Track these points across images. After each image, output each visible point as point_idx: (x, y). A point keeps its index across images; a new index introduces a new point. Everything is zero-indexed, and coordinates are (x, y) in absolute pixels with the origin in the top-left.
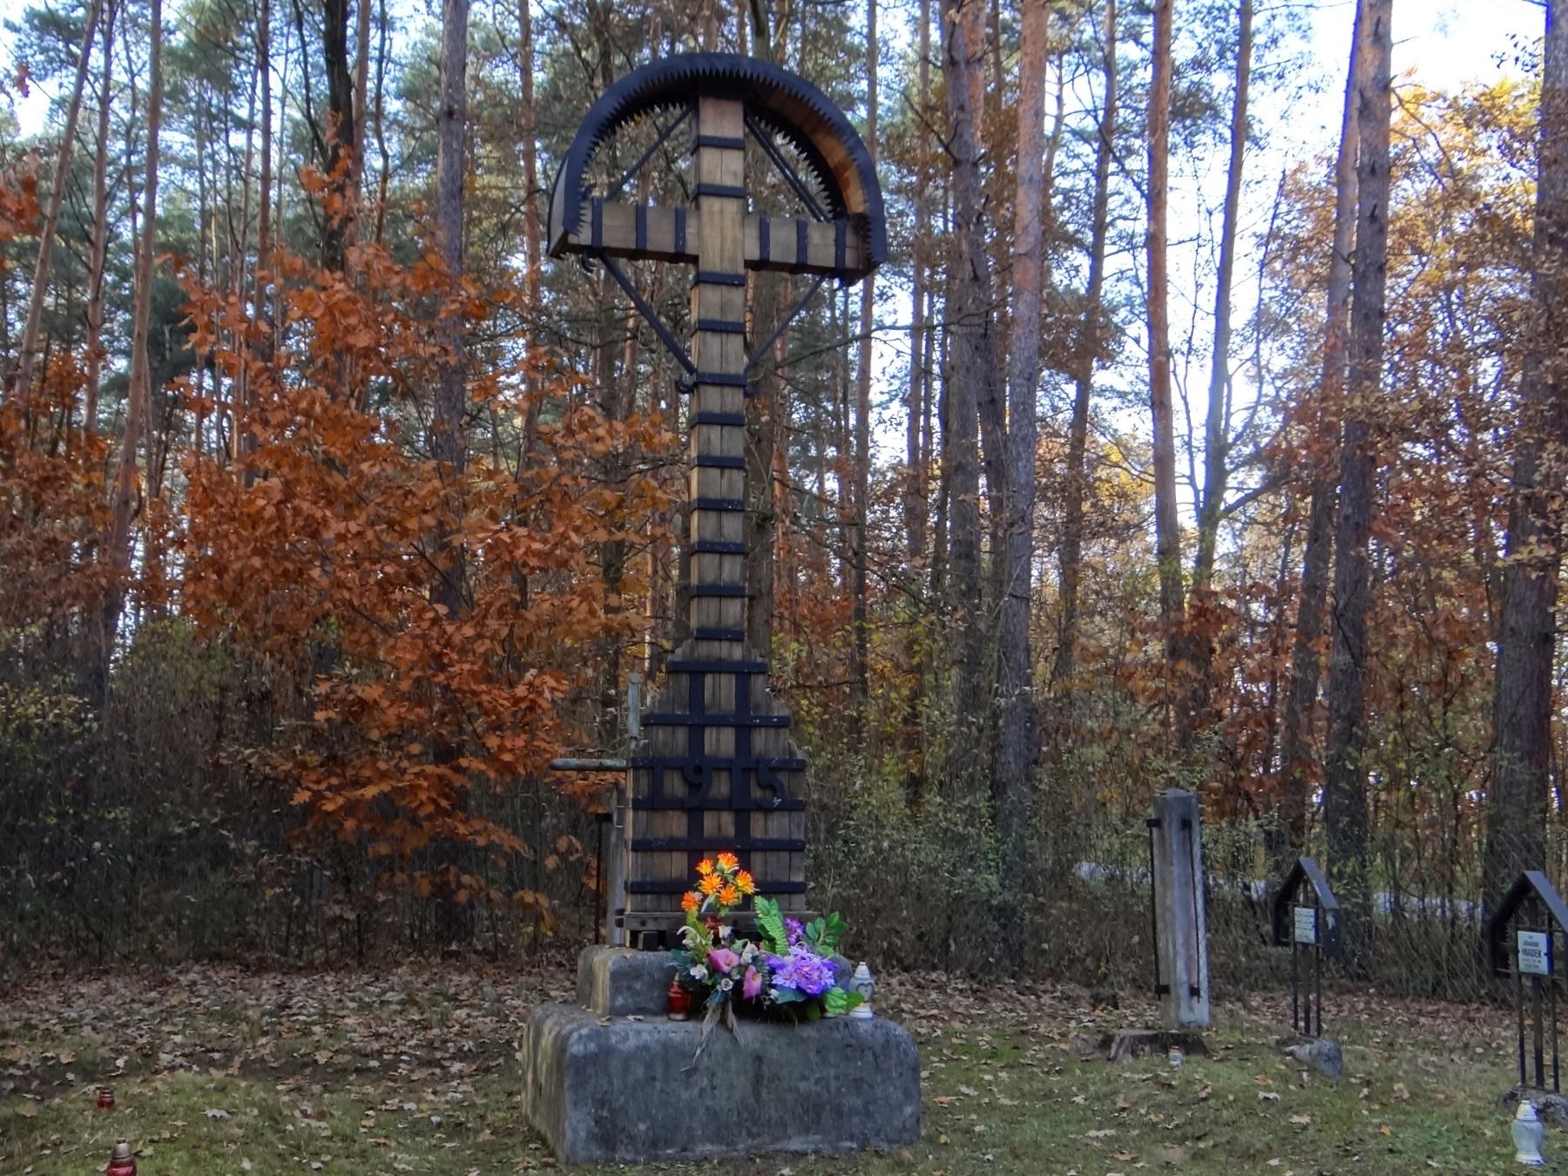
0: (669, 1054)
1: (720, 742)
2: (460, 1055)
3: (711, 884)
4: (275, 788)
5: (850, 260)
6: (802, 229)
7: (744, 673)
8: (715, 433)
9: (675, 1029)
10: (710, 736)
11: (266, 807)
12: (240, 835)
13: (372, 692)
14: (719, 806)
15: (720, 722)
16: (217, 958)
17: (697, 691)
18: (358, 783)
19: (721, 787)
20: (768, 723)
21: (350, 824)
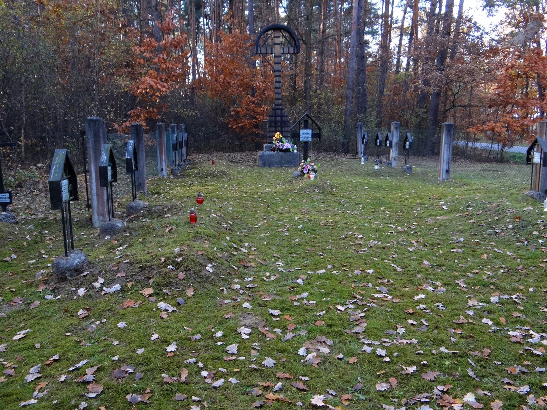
0: (271, 155)
1: (279, 119)
2: (252, 161)
3: (276, 136)
4: (227, 124)
5: (295, 52)
6: (289, 48)
7: (282, 110)
8: (277, 78)
9: (272, 153)
10: (277, 118)
11: (224, 127)
12: (221, 131)
13: (239, 110)
14: (278, 127)
15: (279, 116)
16: (219, 151)
17: (276, 112)
18: (239, 124)
19: (279, 124)
20: (285, 116)
21: (237, 130)
